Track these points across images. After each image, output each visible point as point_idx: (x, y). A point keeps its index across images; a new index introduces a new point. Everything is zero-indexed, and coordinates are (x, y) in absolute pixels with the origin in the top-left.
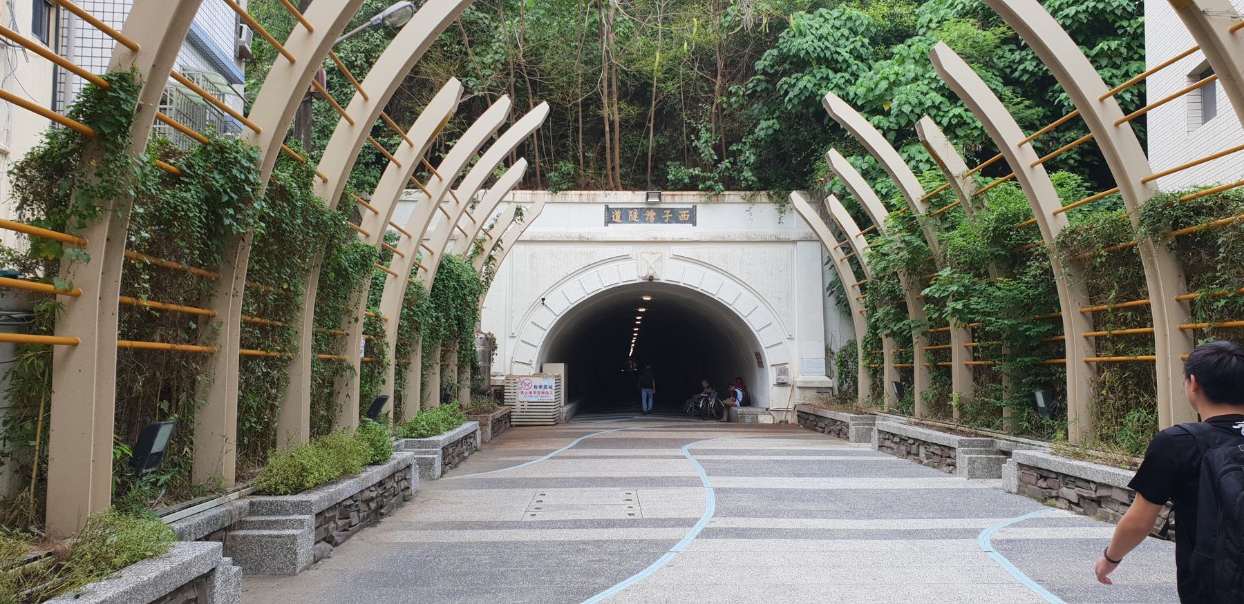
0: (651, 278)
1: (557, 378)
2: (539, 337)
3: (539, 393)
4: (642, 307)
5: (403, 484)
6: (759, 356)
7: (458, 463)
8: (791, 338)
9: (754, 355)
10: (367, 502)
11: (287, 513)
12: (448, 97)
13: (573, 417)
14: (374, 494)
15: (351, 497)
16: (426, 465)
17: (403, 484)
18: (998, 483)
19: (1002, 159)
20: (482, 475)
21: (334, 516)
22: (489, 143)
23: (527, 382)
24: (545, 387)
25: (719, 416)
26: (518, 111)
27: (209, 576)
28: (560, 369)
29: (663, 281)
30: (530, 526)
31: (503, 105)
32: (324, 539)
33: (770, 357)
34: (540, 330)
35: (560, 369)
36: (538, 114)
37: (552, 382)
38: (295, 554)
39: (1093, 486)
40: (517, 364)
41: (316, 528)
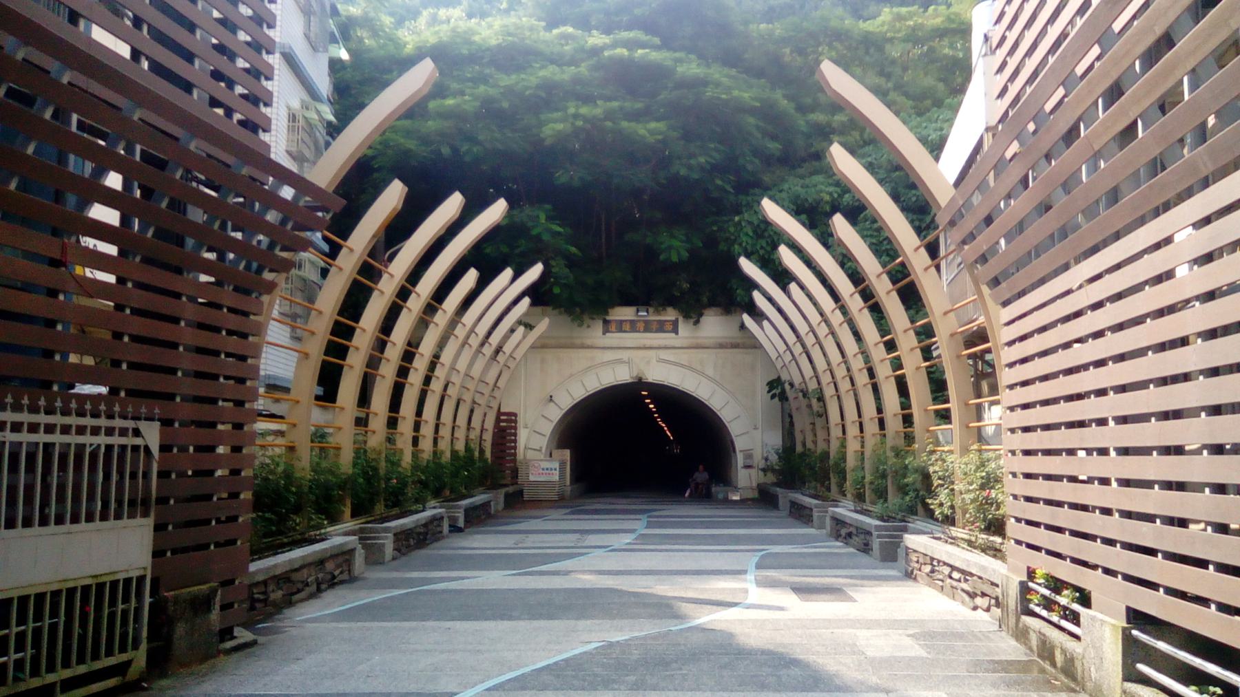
0: (640, 379)
1: (562, 464)
2: (548, 428)
5: (439, 529)
7: (485, 519)
8: (756, 428)
10: (420, 534)
12: (393, 196)
18: (824, 531)
19: (338, 315)
24: (551, 469)
25: (704, 496)
28: (567, 454)
29: (650, 380)
31: (453, 204)
33: (740, 444)
34: (570, 398)
35: (567, 454)
36: (496, 212)
37: (556, 465)
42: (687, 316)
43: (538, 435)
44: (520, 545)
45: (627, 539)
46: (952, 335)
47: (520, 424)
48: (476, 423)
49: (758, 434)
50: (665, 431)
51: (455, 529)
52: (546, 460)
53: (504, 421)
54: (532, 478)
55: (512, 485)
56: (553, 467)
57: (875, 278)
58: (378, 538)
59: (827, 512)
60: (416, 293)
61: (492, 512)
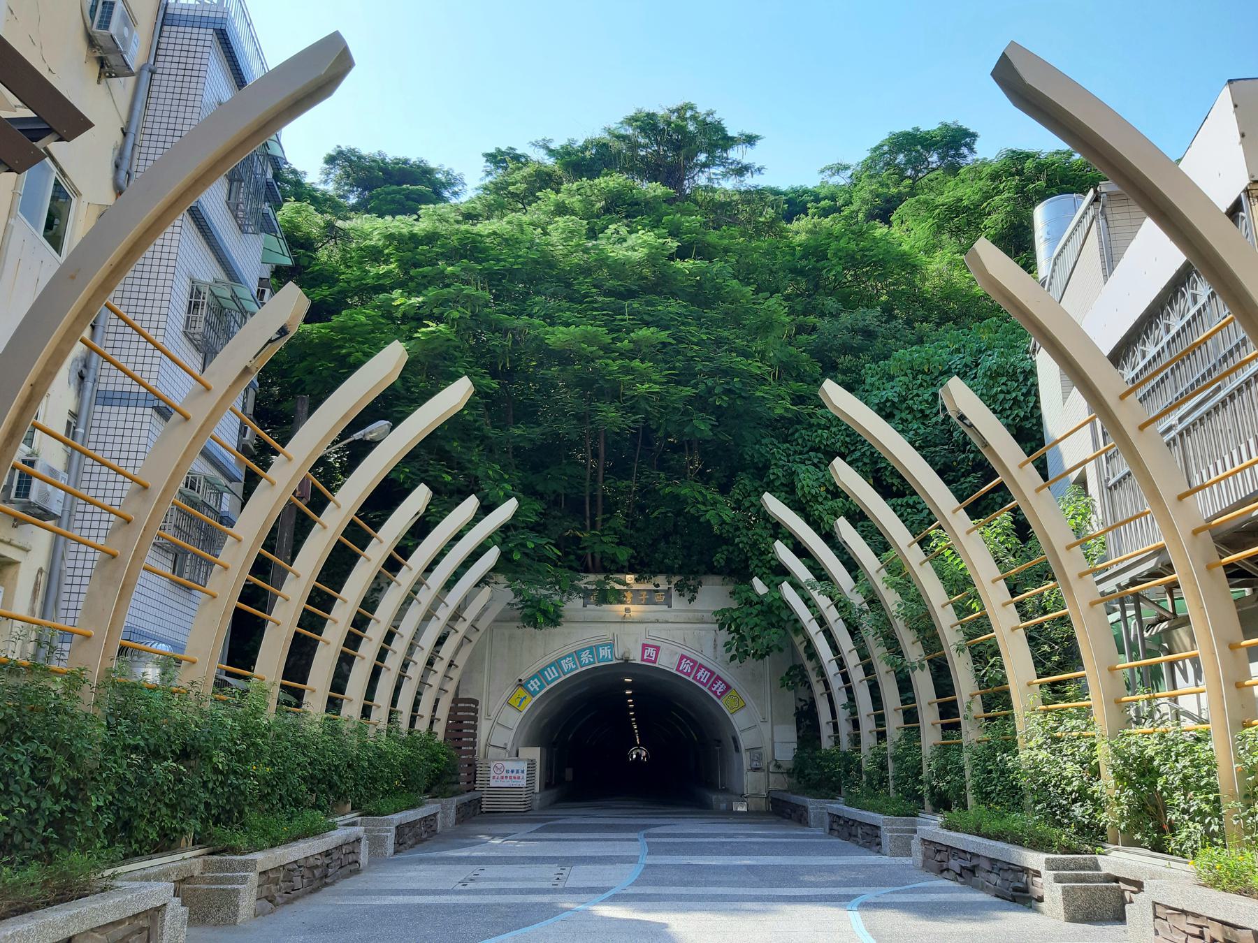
1: (531, 763)
2: (514, 719)
3: (510, 778)
4: (629, 690)
5: (351, 858)
6: (735, 740)
8: (764, 721)
9: (731, 740)
10: (311, 868)
11: (234, 871)
13: (556, 802)
14: (319, 863)
15: (296, 862)
16: (376, 843)
17: (351, 858)
18: (907, 861)
20: (434, 854)
21: (278, 878)
22: (458, 537)
23: (499, 766)
24: (517, 772)
26: (486, 509)
27: (160, 909)
30: (459, 893)
32: (266, 897)
33: (745, 741)
35: (535, 753)
37: (523, 766)
38: (237, 906)
39: (969, 856)
40: (491, 748)
41: (259, 886)
42: (680, 588)
43: (502, 729)
44: (471, 886)
45: (631, 872)
46: (1195, 532)
47: (482, 715)
48: (425, 709)
49: (766, 729)
50: (635, 734)
51: (377, 858)
52: (512, 760)
53: (463, 709)
54: (493, 783)
55: (468, 791)
56: (520, 768)
57: (1017, 468)
58: (232, 881)
59: (915, 832)
60: (335, 502)
61: (439, 829)
